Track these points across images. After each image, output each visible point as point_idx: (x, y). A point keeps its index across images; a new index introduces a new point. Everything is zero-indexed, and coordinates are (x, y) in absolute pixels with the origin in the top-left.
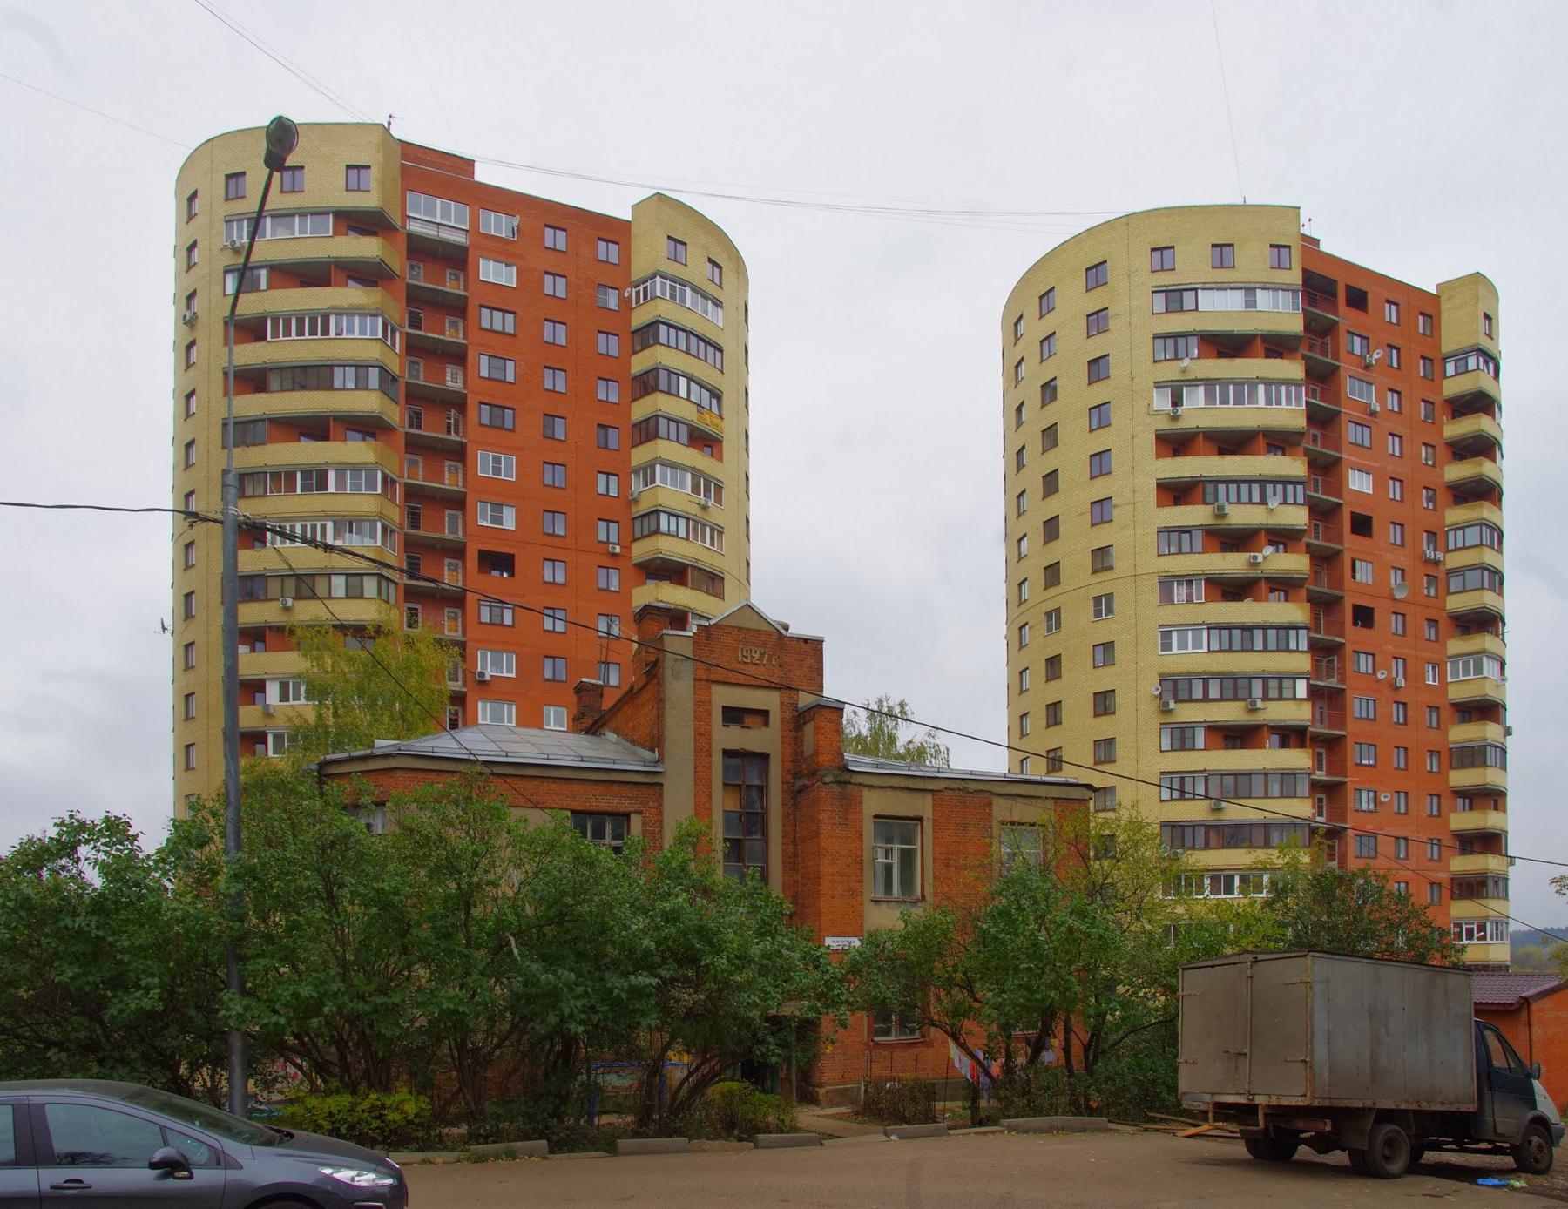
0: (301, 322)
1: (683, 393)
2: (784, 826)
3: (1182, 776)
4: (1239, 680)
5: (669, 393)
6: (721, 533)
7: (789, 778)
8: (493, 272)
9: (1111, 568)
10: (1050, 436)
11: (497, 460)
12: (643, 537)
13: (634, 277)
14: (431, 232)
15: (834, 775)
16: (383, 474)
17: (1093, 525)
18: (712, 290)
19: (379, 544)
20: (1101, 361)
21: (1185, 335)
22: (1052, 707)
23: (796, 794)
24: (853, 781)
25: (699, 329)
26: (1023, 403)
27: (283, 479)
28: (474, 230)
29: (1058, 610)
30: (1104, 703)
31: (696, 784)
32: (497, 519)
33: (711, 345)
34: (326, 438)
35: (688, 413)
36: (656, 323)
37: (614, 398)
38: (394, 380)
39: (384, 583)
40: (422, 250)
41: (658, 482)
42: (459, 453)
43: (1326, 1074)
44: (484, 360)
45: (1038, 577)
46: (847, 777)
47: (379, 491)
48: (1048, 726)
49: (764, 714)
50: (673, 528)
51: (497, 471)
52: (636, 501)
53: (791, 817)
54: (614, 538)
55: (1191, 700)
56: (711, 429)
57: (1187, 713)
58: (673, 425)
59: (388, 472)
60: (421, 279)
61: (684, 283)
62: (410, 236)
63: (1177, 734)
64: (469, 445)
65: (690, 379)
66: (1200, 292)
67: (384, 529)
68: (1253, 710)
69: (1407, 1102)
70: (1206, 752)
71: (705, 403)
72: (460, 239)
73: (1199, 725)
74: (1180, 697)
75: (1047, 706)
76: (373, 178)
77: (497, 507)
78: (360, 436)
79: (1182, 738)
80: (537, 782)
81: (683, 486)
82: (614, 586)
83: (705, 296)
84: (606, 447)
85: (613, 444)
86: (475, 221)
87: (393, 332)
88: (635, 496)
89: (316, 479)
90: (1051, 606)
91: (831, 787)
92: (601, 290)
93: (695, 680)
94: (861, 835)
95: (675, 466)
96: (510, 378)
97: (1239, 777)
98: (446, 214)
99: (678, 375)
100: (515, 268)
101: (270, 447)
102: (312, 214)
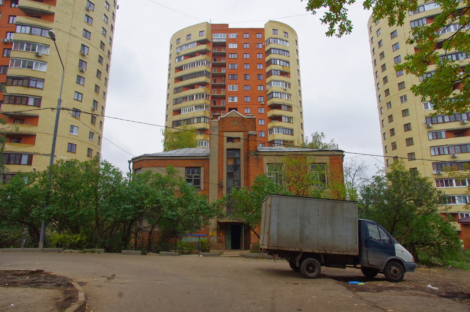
0: (190, 65)
1: (278, 63)
2: (244, 168)
3: (439, 148)
4: (456, 115)
5: (274, 64)
6: (290, 95)
7: (246, 155)
8: (232, 46)
9: (405, 88)
10: (382, 55)
11: (233, 87)
12: (269, 99)
13: (265, 40)
14: (218, 41)
15: (254, 153)
16: (206, 94)
17: (397, 77)
18: (285, 39)
19: (204, 109)
20: (394, 32)
21: (421, 19)
22: (392, 130)
23: (247, 159)
24: (259, 154)
25: (282, 48)
26: (374, 48)
27: (185, 98)
28: (228, 38)
29: (390, 102)
30: (407, 127)
31: (219, 158)
32: (233, 100)
33: (286, 51)
34: (194, 88)
35: (280, 68)
36: (270, 49)
37: (261, 68)
38: (209, 73)
39: (206, 118)
40: (216, 45)
41: (272, 85)
42: (224, 87)
43: (276, 238)
44: (230, 65)
45: (383, 94)
46: (258, 153)
47: (205, 98)
48: (391, 136)
49: (239, 139)
50: (277, 96)
51: (233, 89)
52: (267, 91)
53: (247, 165)
54: (262, 100)
55: (438, 123)
56: (287, 71)
57: (437, 127)
58: (276, 72)
59: (207, 93)
60: (216, 51)
61: (277, 39)
62: (213, 43)
63: (434, 134)
64: (226, 85)
65: (280, 60)
66: (425, 6)
67: (206, 106)
68: (463, 124)
69: (318, 250)
70: (446, 139)
71: (285, 65)
72: (224, 41)
73: (442, 131)
74: (434, 123)
75: (390, 130)
76: (205, 33)
77: (233, 97)
78: (201, 86)
79: (437, 135)
80: (177, 161)
81: (279, 85)
82: (263, 112)
83: (283, 40)
84: (260, 80)
85: (262, 78)
86: (228, 36)
87: (209, 63)
88: (267, 89)
89: (192, 97)
90: (388, 101)
91: (253, 156)
92: (258, 44)
93: (219, 131)
94: (263, 169)
95: (277, 81)
96: (236, 68)
97: (462, 146)
98: (221, 36)
99: (277, 60)
100: (237, 44)
101: (183, 92)
102: (192, 43)
